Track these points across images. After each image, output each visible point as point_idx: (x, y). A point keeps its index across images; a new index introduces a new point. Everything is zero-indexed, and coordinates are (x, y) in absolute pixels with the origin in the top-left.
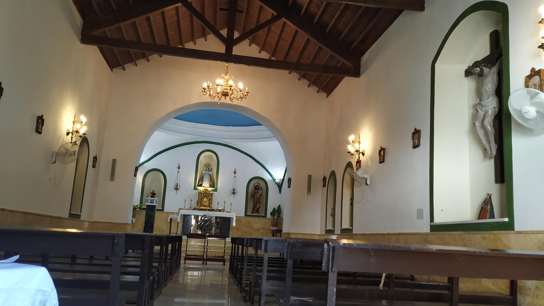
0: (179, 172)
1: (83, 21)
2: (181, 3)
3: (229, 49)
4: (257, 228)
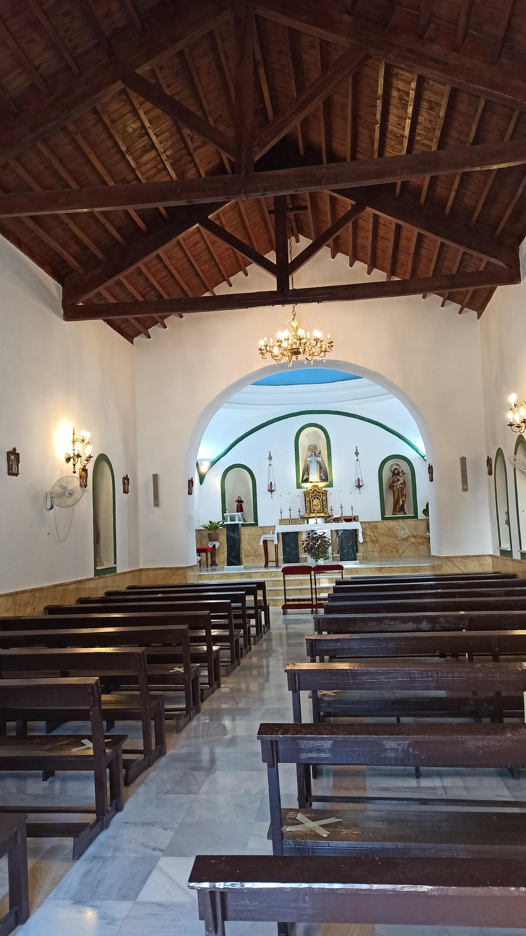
0: (270, 465)
1: (62, 286)
2: (198, 224)
3: (283, 283)
4: (405, 536)
